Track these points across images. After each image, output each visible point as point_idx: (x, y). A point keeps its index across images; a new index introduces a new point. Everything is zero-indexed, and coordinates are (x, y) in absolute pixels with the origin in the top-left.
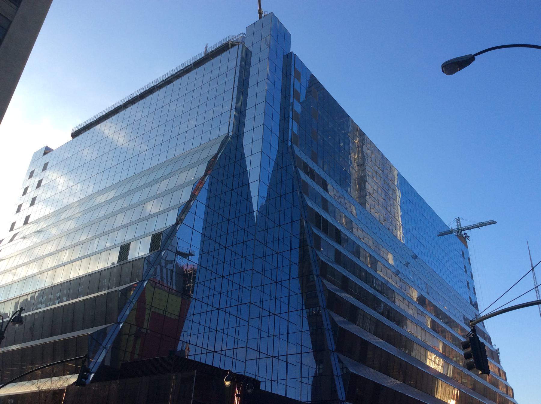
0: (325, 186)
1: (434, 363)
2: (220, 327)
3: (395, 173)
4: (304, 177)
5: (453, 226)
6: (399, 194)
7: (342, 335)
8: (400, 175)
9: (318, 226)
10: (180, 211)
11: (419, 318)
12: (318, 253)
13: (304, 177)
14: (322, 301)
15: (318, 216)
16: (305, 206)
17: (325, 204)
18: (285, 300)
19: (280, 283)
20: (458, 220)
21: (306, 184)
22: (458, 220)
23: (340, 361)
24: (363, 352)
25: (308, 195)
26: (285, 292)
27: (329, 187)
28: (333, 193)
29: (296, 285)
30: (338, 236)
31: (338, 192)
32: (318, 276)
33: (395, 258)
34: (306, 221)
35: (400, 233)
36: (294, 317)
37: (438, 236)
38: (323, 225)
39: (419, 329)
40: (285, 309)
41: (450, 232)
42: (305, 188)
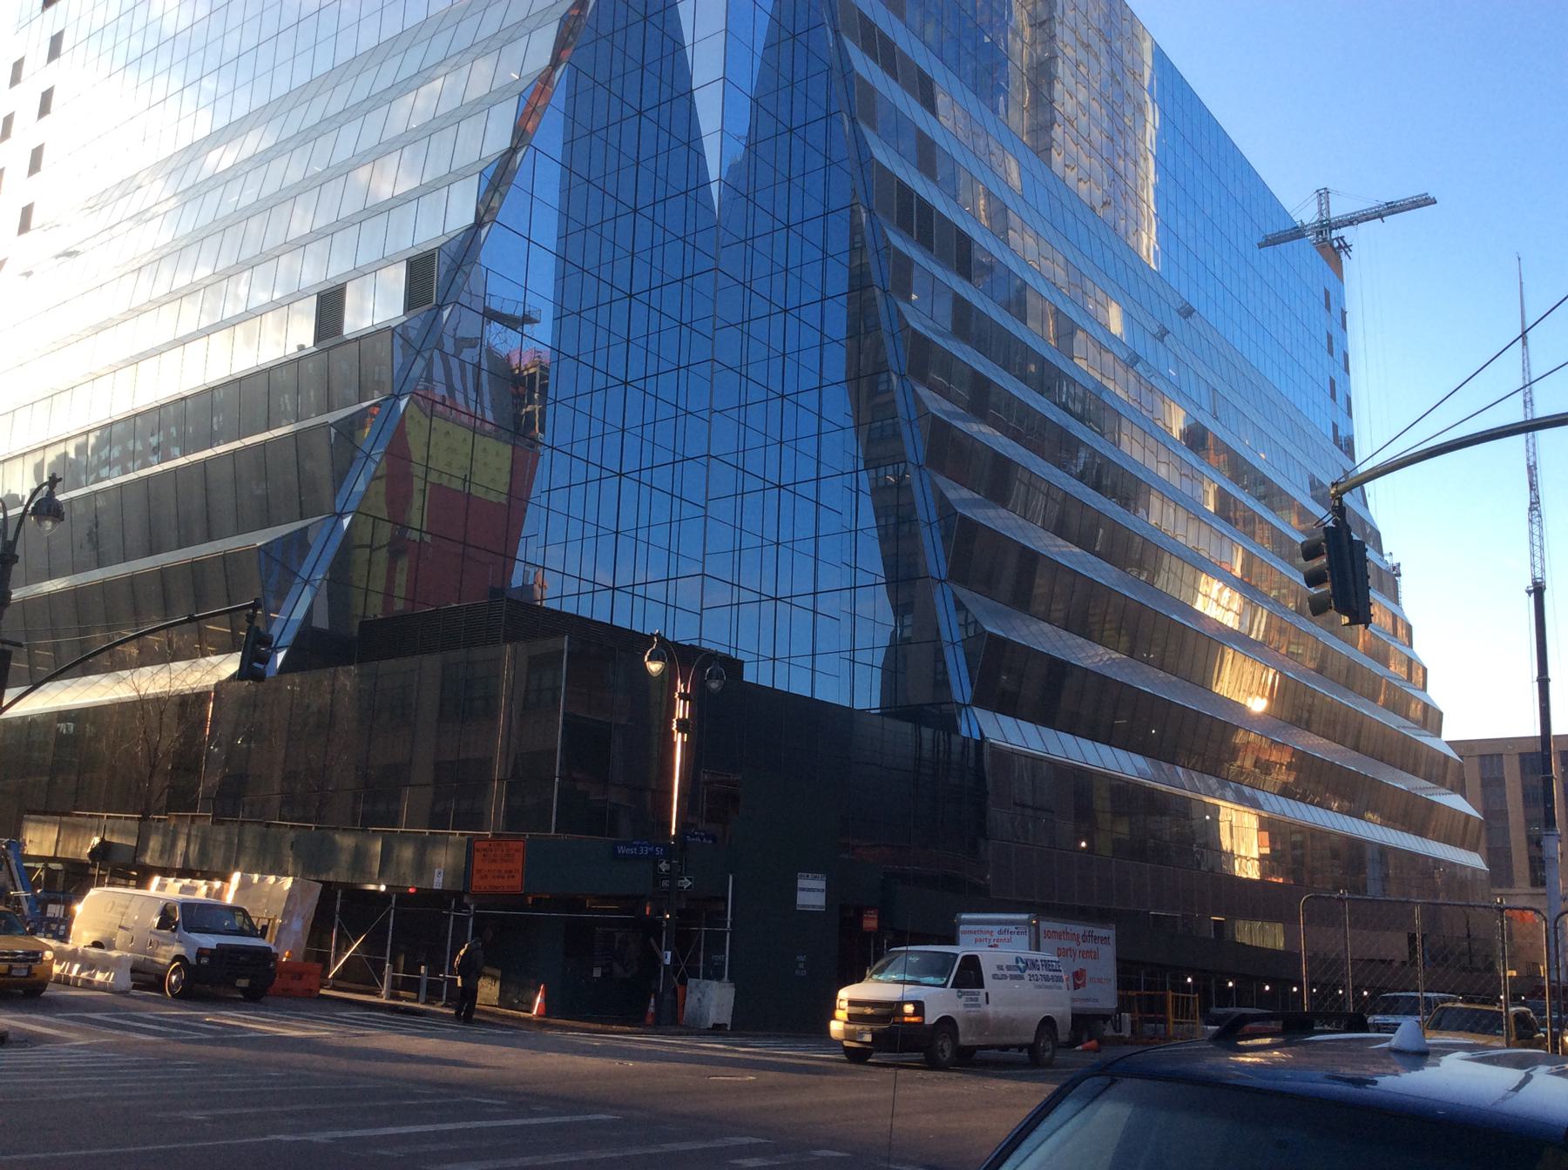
0: (926, 94)
1: (1217, 603)
2: (627, 522)
3: (1147, 46)
4: (864, 66)
5: (1306, 215)
6: (1152, 118)
7: (965, 538)
8: (1159, 54)
9: (904, 225)
10: (485, 184)
11: (1187, 487)
12: (903, 306)
13: (864, 66)
14: (914, 445)
15: (905, 191)
16: (865, 161)
17: (926, 154)
18: (809, 446)
19: (793, 398)
20: (1323, 195)
21: (869, 90)
22: (1323, 195)
23: (959, 606)
24: (1022, 579)
25: (872, 125)
26: (808, 423)
27: (942, 100)
28: (951, 118)
29: (838, 404)
30: (962, 255)
31: (967, 113)
32: (901, 376)
33: (1128, 316)
34: (869, 211)
35: (1148, 243)
36: (835, 493)
37: (1260, 246)
38: (918, 218)
39: (1181, 514)
40: (807, 470)
41: (1298, 233)
42: (864, 103)
